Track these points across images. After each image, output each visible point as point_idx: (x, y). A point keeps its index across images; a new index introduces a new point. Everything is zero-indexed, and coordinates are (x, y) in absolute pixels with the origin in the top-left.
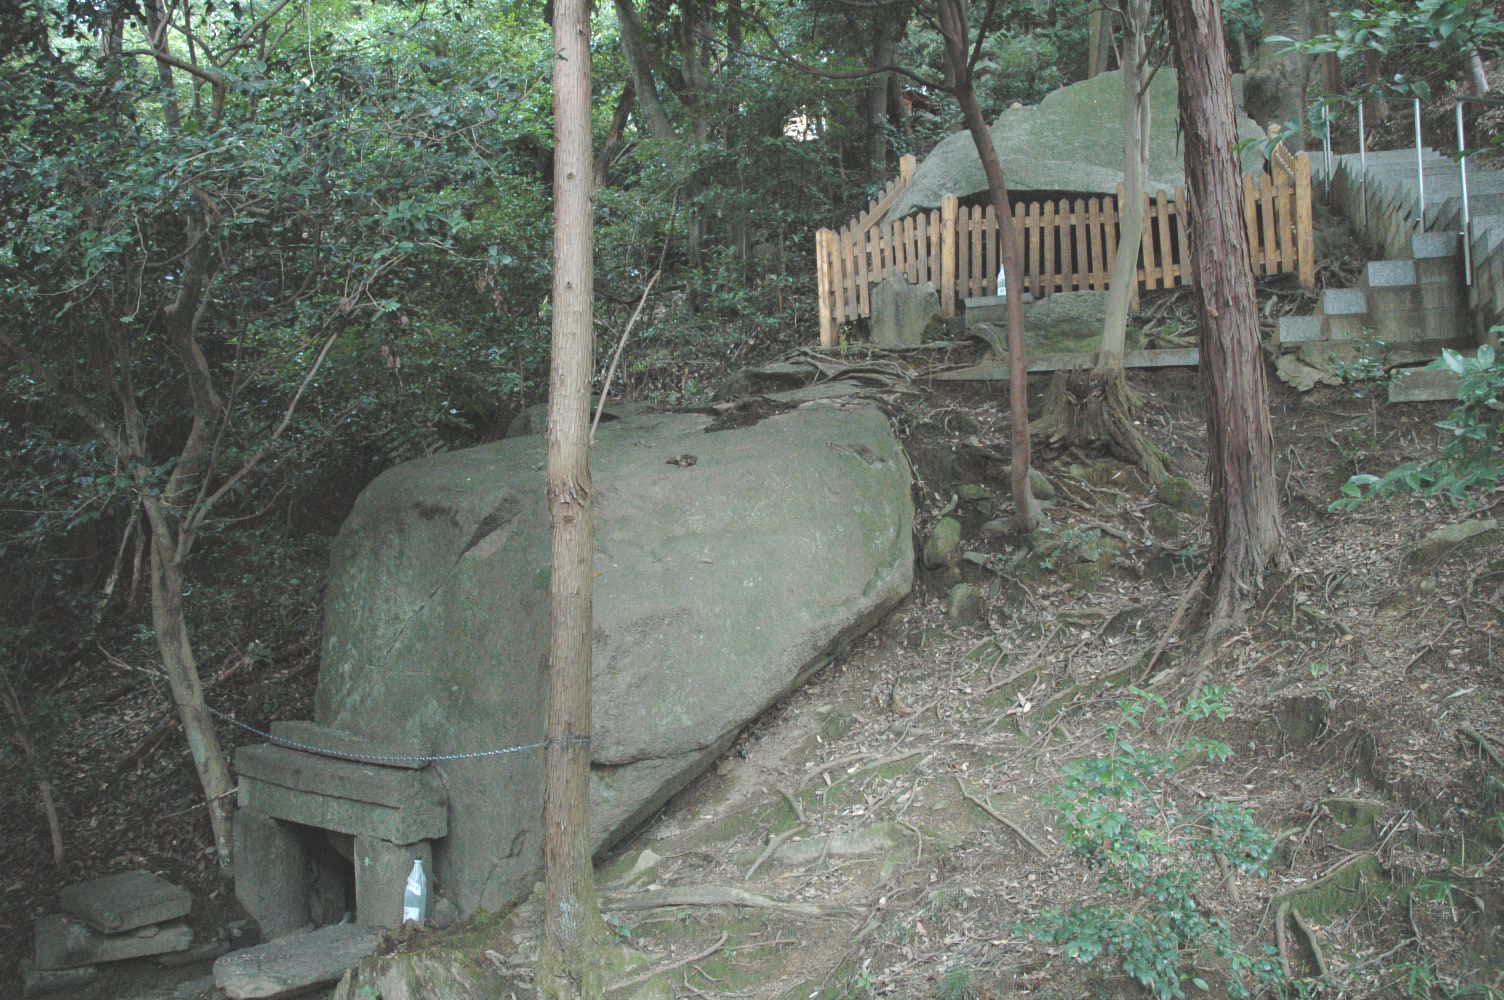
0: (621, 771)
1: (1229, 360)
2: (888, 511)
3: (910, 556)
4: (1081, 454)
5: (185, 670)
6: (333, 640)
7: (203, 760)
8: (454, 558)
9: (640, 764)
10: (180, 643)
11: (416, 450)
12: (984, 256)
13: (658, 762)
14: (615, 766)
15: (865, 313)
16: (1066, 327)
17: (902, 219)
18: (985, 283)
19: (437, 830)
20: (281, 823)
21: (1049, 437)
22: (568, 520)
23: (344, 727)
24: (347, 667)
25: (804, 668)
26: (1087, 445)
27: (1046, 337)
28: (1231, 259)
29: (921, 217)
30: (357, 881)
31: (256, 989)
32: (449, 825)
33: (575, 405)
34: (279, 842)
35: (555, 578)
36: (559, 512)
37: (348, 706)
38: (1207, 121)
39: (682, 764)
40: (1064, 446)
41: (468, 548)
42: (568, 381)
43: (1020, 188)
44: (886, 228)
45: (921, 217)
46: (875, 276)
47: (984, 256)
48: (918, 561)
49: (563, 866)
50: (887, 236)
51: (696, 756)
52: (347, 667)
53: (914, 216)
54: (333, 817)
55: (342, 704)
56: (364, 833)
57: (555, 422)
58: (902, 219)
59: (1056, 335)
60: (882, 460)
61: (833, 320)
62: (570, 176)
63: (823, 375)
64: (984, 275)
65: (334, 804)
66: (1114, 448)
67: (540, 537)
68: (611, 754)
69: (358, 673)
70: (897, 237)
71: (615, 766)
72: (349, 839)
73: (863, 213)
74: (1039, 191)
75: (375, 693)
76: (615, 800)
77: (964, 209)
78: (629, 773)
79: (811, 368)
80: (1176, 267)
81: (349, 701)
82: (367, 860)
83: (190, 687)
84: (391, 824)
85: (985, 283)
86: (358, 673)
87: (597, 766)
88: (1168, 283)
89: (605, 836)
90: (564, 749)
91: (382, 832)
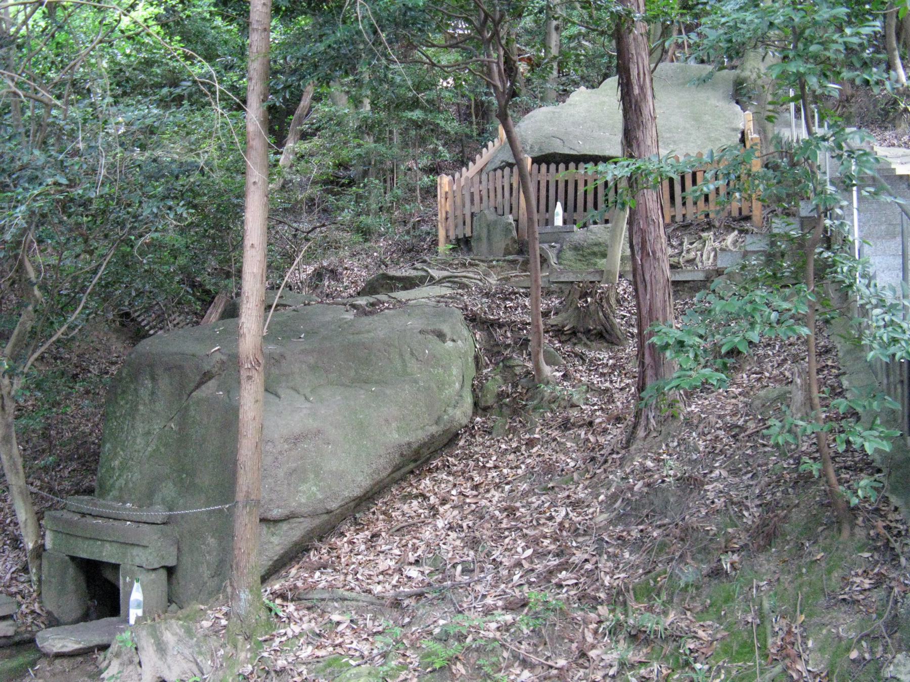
0: (280, 524)
1: (649, 288)
2: (454, 372)
3: (469, 400)
4: (584, 339)
5: (15, 464)
6: (108, 445)
7: (24, 519)
8: (185, 397)
9: (291, 520)
10: (12, 445)
11: (161, 321)
12: (547, 197)
13: (302, 520)
14: (276, 521)
15: (468, 234)
16: (596, 249)
17: (495, 170)
18: (547, 216)
19: (171, 562)
20: (73, 558)
21: (563, 327)
22: (249, 378)
23: (115, 499)
24: (117, 463)
25: (397, 468)
26: (588, 332)
27: (583, 256)
28: (652, 228)
29: (507, 170)
30: (121, 591)
31: (63, 647)
32: (178, 559)
33: (255, 313)
34: (71, 571)
35: (241, 411)
36: (244, 374)
37: (117, 487)
38: (638, 146)
39: (317, 521)
40: (574, 333)
41: (194, 390)
42: (251, 300)
43: (572, 152)
44: (484, 177)
45: (507, 170)
46: (476, 209)
47: (547, 197)
48: (476, 404)
49: (242, 573)
50: (484, 182)
51: (325, 517)
52: (117, 463)
53: (502, 168)
54: (107, 554)
55: (113, 486)
56: (126, 564)
57: (243, 323)
58: (495, 170)
59: (589, 254)
60: (454, 341)
61: (447, 237)
62: (255, 183)
63: (432, 278)
64: (547, 211)
65: (107, 545)
66: (605, 334)
67: (233, 385)
68: (276, 513)
69: (123, 467)
70: (491, 183)
71: (276, 521)
72: (116, 567)
73: (471, 164)
74: (585, 155)
75: (134, 479)
76: (278, 542)
77: (535, 165)
78: (285, 526)
79: (424, 274)
80: (672, 209)
81: (117, 485)
82: (128, 579)
83: (17, 473)
84: (140, 557)
85: (547, 216)
86: (123, 467)
87: (263, 520)
88: (679, 218)
89: (271, 563)
90: (245, 507)
91: (137, 561)
